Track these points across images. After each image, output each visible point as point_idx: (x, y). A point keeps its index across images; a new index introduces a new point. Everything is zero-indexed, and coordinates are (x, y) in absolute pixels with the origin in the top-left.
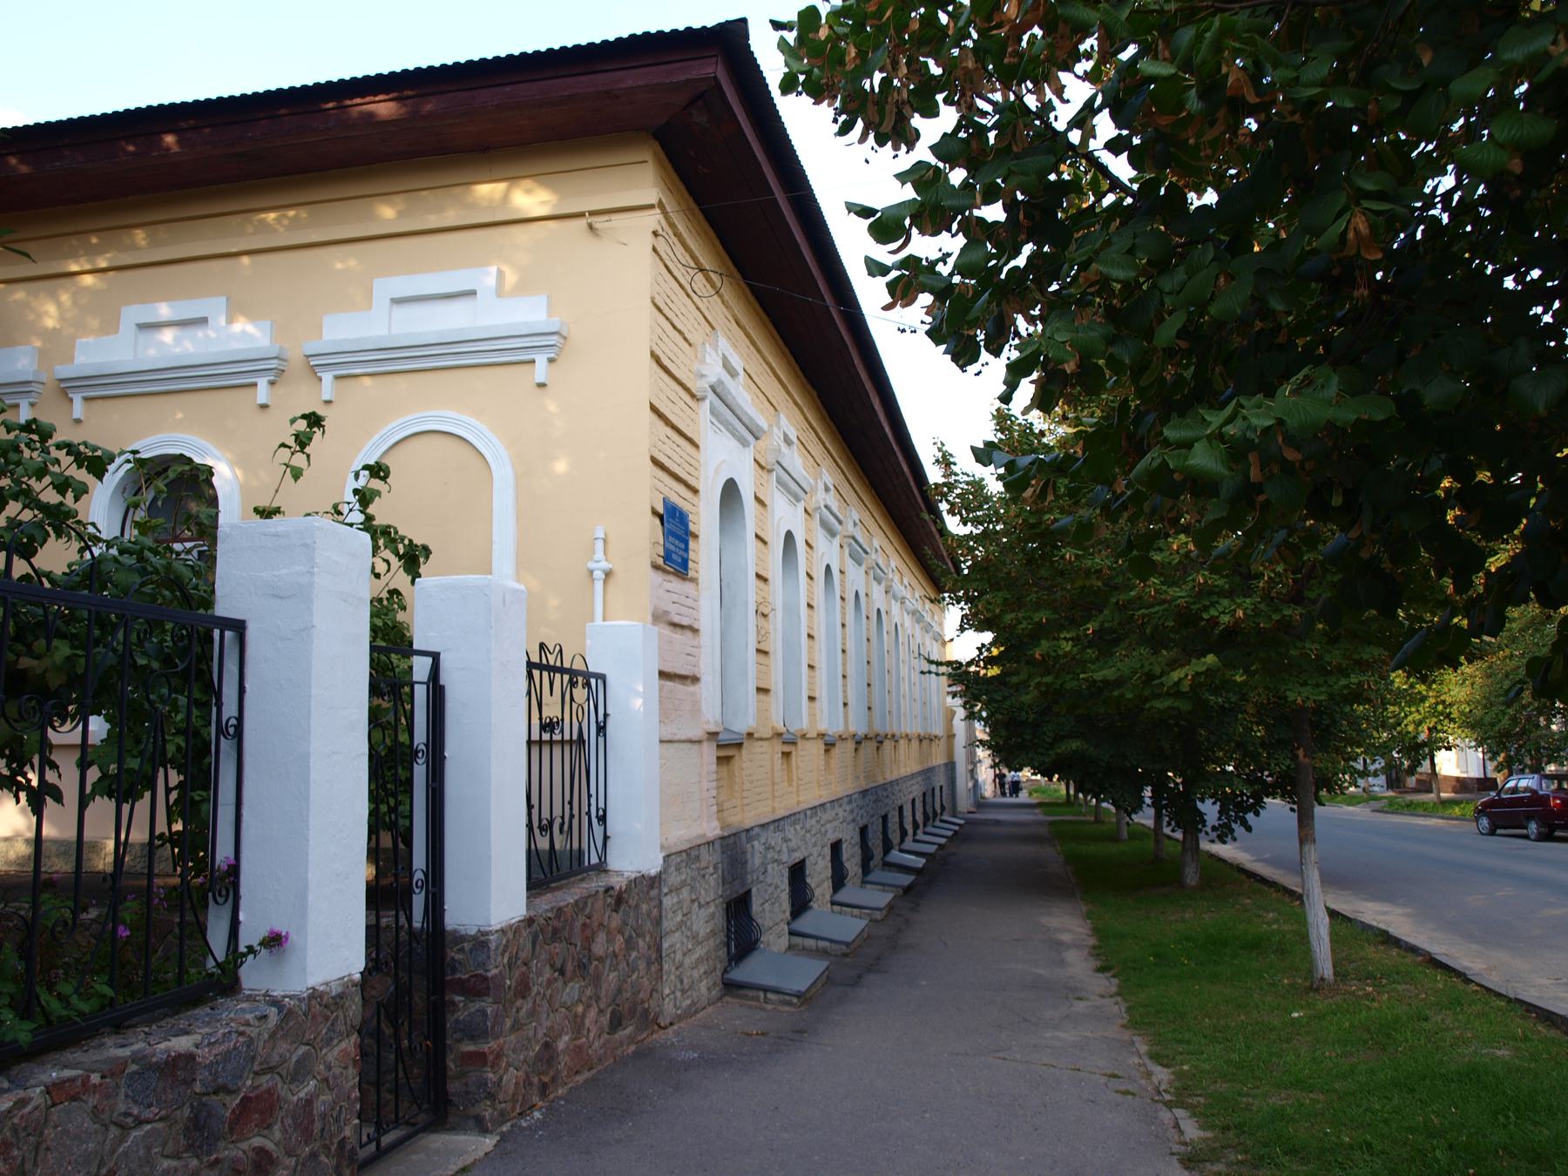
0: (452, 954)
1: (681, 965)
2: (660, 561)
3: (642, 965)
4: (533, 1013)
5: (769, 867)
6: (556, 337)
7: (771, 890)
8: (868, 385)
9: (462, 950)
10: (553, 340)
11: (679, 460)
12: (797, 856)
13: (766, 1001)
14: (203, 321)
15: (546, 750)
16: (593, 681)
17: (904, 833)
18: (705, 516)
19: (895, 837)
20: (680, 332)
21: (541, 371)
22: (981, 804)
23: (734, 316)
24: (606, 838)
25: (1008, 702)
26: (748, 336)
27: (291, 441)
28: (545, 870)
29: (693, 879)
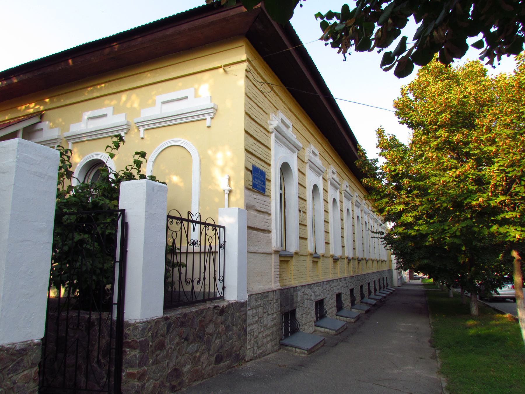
0: (126, 331)
1: (257, 337)
2: (251, 187)
3: (235, 337)
4: (166, 357)
5: (305, 301)
6: (212, 110)
7: (306, 310)
8: (346, 137)
9: (129, 329)
10: (212, 110)
11: (261, 153)
12: (320, 298)
13: (296, 352)
14: (106, 115)
15: (211, 255)
16: (218, 229)
17: (370, 293)
18: (274, 174)
19: (366, 294)
20: (261, 108)
21: (208, 122)
22: (404, 284)
23: (288, 107)
24: (224, 288)
25: (408, 249)
26: (295, 115)
27: (113, 146)
28: (173, 298)
29: (264, 304)
